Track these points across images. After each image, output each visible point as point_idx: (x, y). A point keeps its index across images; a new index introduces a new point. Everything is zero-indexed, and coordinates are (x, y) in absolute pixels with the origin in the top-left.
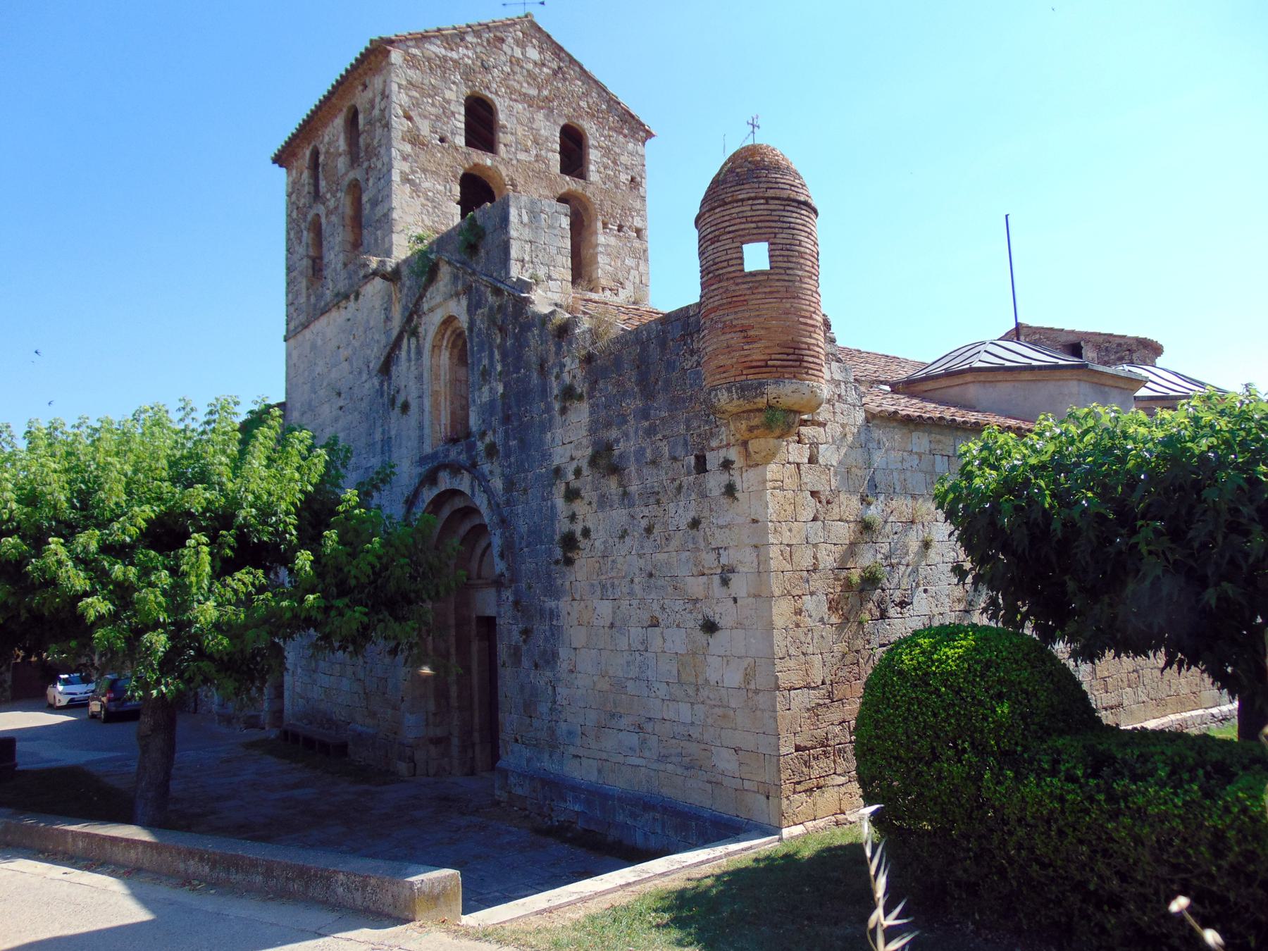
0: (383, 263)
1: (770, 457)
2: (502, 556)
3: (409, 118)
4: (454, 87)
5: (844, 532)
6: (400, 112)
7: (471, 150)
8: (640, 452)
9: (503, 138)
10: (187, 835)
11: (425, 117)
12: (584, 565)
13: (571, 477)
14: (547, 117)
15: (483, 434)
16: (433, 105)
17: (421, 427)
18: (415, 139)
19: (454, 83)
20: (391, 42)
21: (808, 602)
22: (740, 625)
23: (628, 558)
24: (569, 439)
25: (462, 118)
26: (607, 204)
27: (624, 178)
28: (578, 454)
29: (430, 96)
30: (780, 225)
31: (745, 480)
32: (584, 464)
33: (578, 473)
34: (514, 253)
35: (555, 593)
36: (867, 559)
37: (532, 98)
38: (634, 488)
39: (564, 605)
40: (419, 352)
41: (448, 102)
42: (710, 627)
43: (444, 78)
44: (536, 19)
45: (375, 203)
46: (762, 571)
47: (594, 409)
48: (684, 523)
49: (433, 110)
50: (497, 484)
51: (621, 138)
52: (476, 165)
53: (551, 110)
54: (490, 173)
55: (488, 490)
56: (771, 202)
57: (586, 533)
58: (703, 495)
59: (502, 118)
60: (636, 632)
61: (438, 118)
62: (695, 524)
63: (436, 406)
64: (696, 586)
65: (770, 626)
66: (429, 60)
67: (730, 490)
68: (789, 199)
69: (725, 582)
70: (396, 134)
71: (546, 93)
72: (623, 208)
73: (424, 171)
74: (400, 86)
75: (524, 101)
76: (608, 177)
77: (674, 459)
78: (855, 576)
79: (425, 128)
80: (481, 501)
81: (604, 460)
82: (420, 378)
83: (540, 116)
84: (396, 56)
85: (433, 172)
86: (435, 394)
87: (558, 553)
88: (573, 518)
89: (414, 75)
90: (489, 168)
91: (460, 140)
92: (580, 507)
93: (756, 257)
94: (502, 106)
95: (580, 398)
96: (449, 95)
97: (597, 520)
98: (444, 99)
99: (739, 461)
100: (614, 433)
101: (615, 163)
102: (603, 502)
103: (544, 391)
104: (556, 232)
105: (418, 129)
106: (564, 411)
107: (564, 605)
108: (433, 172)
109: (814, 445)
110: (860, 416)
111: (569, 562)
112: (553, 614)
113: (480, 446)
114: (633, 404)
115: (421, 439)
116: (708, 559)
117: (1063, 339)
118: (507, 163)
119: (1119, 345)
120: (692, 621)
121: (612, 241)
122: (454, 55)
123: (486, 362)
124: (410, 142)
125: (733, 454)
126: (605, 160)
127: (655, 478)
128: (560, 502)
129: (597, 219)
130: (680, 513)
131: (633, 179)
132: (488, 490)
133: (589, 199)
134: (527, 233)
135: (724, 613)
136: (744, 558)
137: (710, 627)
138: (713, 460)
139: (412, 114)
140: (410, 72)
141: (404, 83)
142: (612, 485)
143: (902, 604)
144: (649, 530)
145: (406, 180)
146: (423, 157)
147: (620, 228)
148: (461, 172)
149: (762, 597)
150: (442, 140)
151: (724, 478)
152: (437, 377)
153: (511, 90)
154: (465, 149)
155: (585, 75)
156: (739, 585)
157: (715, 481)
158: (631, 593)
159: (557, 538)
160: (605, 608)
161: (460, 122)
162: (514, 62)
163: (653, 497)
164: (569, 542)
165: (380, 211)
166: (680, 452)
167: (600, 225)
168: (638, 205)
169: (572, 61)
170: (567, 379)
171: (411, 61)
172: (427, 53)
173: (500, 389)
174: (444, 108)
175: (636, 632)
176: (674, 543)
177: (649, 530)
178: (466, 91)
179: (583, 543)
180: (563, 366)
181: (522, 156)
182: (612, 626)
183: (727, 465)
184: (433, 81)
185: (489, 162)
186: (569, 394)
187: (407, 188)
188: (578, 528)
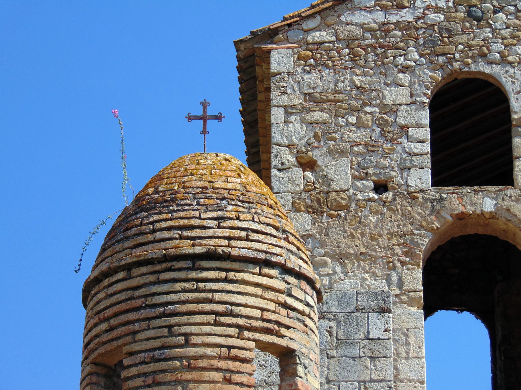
3: (308, 164)
4: (404, 78)
6: (290, 159)
7: (445, 192)
11: (343, 153)
16: (359, 125)
19: (405, 69)
20: (271, 35)
25: (425, 133)
29: (351, 110)
30: (144, 313)
43: (382, 67)
49: (360, 135)
52: (462, 217)
54: (501, 224)
56: (135, 271)
61: (370, 147)
66: (350, 42)
68: (166, 258)
73: (341, 258)
74: (289, 110)
79: (340, 174)
85: (360, 257)
89: (318, 81)
90: (493, 216)
91: (421, 178)
96: (392, 95)
98: (382, 106)
104: (356, 351)
105: (327, 180)
108: (360, 257)
124: (311, 210)
139: (314, 155)
140: (311, 79)
141: (297, 101)
146: (336, 232)
148: (424, 242)
150: (381, 187)
154: (432, 193)
161: (420, 142)
171: (313, 57)
172: (345, 31)
174: (382, 124)
178: (431, 77)
184: (358, 80)
185: (488, 205)
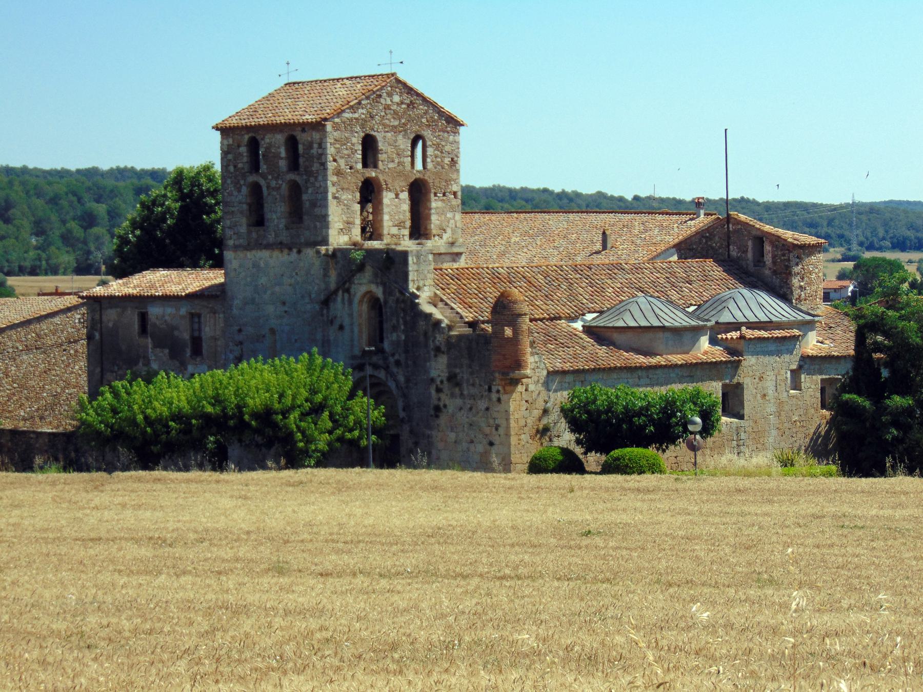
0: (327, 250)
1: (513, 391)
2: (404, 410)
5: (537, 413)
8: (468, 380)
9: (382, 157)
10: (399, 476)
12: (443, 420)
13: (439, 383)
14: (404, 137)
15: (393, 355)
17: (352, 340)
18: (338, 173)
20: (326, 119)
21: (523, 436)
22: (501, 444)
23: (463, 418)
24: (439, 367)
26: (437, 181)
27: (447, 160)
28: (442, 374)
31: (504, 397)
32: (445, 379)
33: (442, 382)
34: (411, 278)
35: (430, 428)
36: (545, 421)
37: (395, 127)
38: (465, 392)
39: (434, 433)
40: (351, 302)
41: (353, 145)
42: (491, 444)
44: (402, 77)
45: (314, 204)
46: (508, 427)
47: (449, 359)
48: (483, 409)
49: (346, 152)
50: (401, 379)
51: (446, 135)
53: (405, 131)
55: (396, 380)
57: (445, 406)
58: (490, 399)
59: (381, 146)
60: (465, 445)
62: (487, 409)
63: (360, 332)
64: (487, 430)
65: (510, 445)
66: (344, 123)
67: (499, 400)
69: (497, 429)
70: (330, 172)
71: (403, 121)
72: (446, 181)
75: (392, 131)
76: (438, 164)
77: (481, 385)
78: (541, 427)
80: (392, 385)
81: (452, 378)
82: (351, 315)
83: (400, 137)
84: (329, 126)
86: (360, 325)
87: (432, 412)
88: (439, 399)
92: (443, 396)
93: (508, 332)
94: (379, 137)
95: (443, 353)
97: (451, 403)
99: (502, 391)
100: (458, 370)
101: (442, 152)
102: (453, 395)
103: (426, 346)
106: (436, 356)
107: (434, 433)
109: (527, 385)
110: (545, 373)
111: (437, 416)
112: (429, 437)
113: (391, 360)
114: (465, 361)
115: (352, 346)
116: (491, 421)
117: (754, 233)
118: (383, 172)
119: (783, 245)
120: (485, 442)
121: (440, 204)
122: (356, 115)
123: (394, 321)
124: (337, 175)
125: (500, 388)
126: (436, 152)
127: (473, 391)
128: (433, 392)
129: (430, 192)
130: (482, 404)
131: (452, 159)
132: (396, 380)
133: (426, 181)
134: (415, 267)
135: (496, 440)
136: (503, 423)
137: (491, 444)
138: (494, 389)
142: (457, 390)
143: (558, 436)
144: (471, 409)
145: (335, 198)
147: (444, 195)
149: (508, 435)
151: (497, 395)
152: (360, 316)
153: (385, 126)
155: (425, 100)
156: (501, 431)
157: (494, 396)
158: (463, 431)
159: (432, 406)
160: (452, 436)
162: (387, 107)
163: (473, 397)
164: (437, 409)
165: (317, 211)
166: (482, 383)
167: (432, 195)
168: (454, 176)
169: (419, 95)
170: (437, 343)
171: (336, 127)
172: (344, 119)
173: (403, 337)
175: (465, 445)
176: (480, 414)
177: (471, 409)
178: (362, 134)
179: (444, 410)
180: (435, 338)
181: (391, 165)
182: (455, 442)
183: (498, 391)
185: (374, 174)
186: (438, 350)
187: (335, 201)
188: (441, 404)
